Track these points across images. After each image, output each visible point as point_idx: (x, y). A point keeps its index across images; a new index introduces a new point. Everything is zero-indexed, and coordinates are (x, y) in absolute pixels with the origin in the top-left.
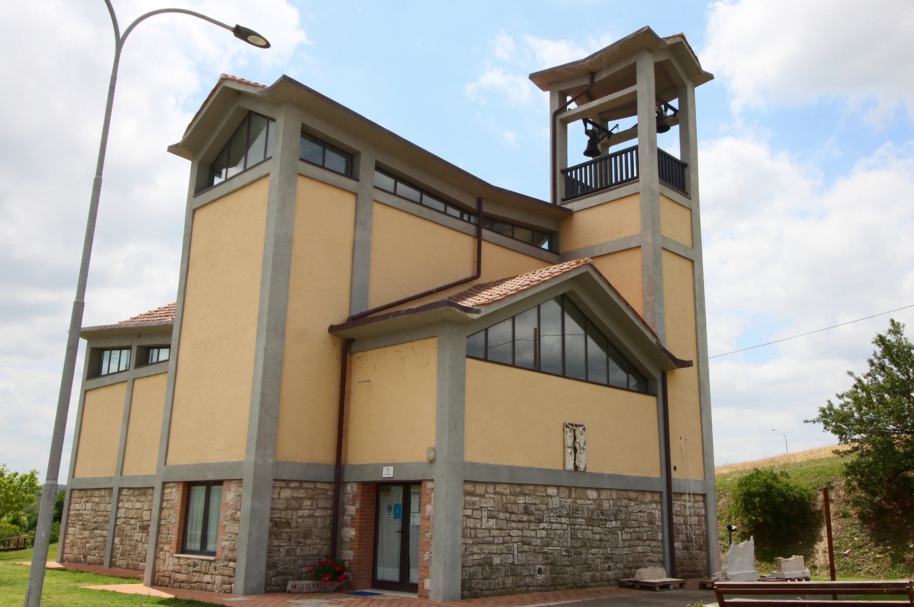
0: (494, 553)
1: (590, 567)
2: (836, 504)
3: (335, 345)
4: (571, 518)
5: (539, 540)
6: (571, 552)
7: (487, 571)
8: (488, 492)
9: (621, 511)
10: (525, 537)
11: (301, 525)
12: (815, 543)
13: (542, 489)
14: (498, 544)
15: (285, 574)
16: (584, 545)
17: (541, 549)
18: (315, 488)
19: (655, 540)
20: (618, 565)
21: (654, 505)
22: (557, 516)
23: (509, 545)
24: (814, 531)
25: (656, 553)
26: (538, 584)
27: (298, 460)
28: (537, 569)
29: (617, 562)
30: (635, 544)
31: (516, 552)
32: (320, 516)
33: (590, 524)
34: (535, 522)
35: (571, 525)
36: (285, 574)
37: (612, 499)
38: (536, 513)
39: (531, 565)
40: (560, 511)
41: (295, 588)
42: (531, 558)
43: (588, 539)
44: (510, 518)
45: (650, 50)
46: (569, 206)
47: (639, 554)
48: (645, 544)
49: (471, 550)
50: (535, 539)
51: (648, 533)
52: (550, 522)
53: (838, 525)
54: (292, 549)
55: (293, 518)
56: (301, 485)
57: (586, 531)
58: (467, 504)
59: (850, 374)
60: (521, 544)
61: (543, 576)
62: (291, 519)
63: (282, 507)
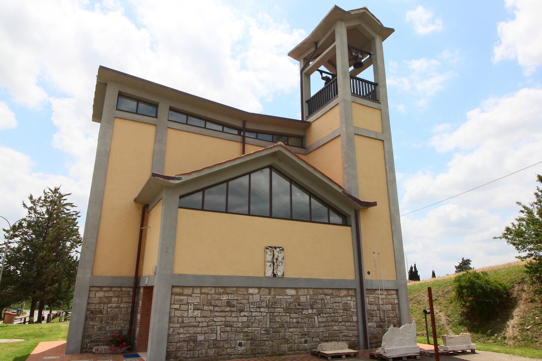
0: (199, 333)
1: (288, 341)
2: (527, 293)
3: (139, 208)
4: (269, 309)
5: (241, 324)
6: (270, 331)
7: (191, 345)
8: (195, 292)
9: (317, 302)
10: (227, 322)
11: (110, 312)
12: (508, 321)
13: (244, 290)
14: (202, 327)
15: (97, 342)
16: (282, 326)
17: (241, 330)
18: (121, 290)
19: (350, 322)
20: (314, 339)
21: (349, 298)
22: (257, 307)
23: (213, 327)
24: (509, 311)
25: (351, 330)
26: (239, 353)
27: (110, 275)
28: (238, 343)
29: (313, 338)
30: (330, 325)
31: (219, 332)
32: (124, 307)
33: (288, 312)
34: (237, 312)
35: (270, 313)
36: (97, 342)
37: (310, 295)
38: (238, 306)
39: (232, 341)
40: (259, 304)
41: (97, 351)
42: (232, 336)
43: (286, 322)
44: (213, 309)
45: (342, 20)
46: (308, 120)
47: (334, 331)
48: (340, 324)
49: (177, 331)
50: (237, 323)
51: (343, 317)
52: (250, 311)
53: (526, 307)
54: (103, 327)
55: (105, 308)
56: (101, 289)
57: (284, 317)
58: (175, 301)
59: (519, 203)
60: (224, 326)
61: (243, 348)
62: (103, 309)
63: (97, 302)
